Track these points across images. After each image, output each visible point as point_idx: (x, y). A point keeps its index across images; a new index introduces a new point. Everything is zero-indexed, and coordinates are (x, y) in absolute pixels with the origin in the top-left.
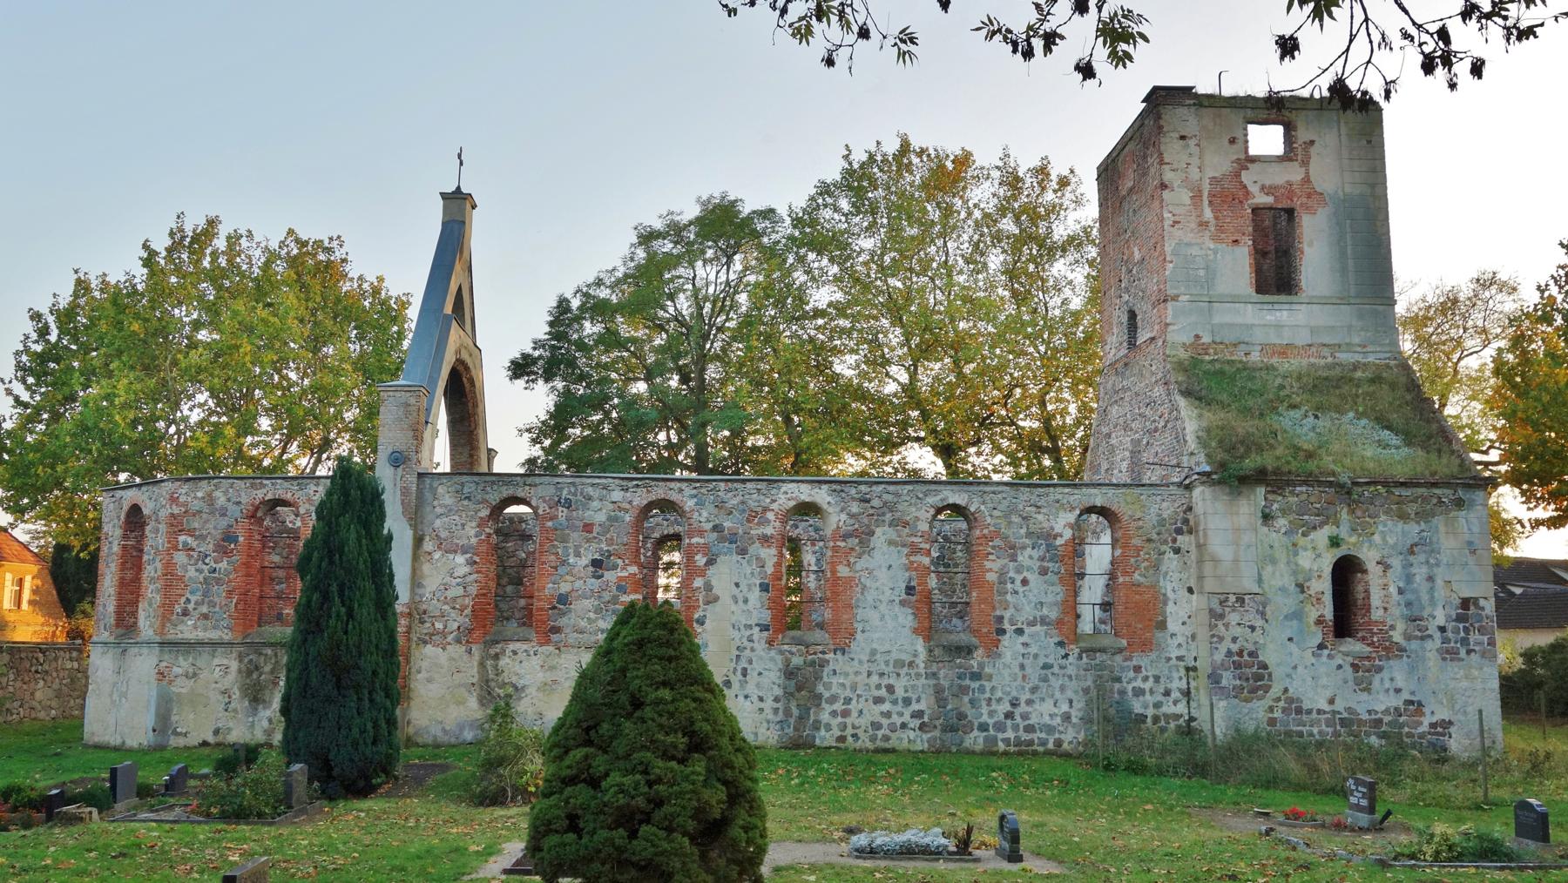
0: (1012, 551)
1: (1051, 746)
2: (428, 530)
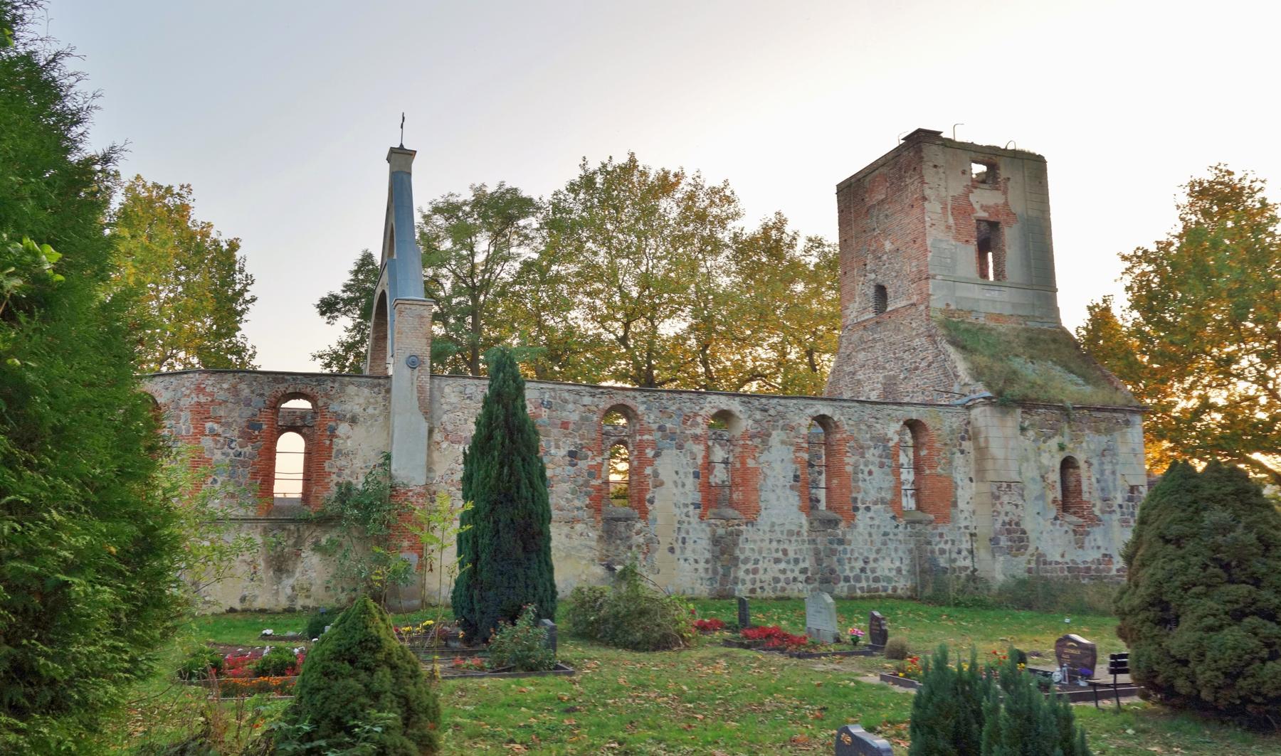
0: (861, 450)
1: (890, 592)
2: (437, 424)
